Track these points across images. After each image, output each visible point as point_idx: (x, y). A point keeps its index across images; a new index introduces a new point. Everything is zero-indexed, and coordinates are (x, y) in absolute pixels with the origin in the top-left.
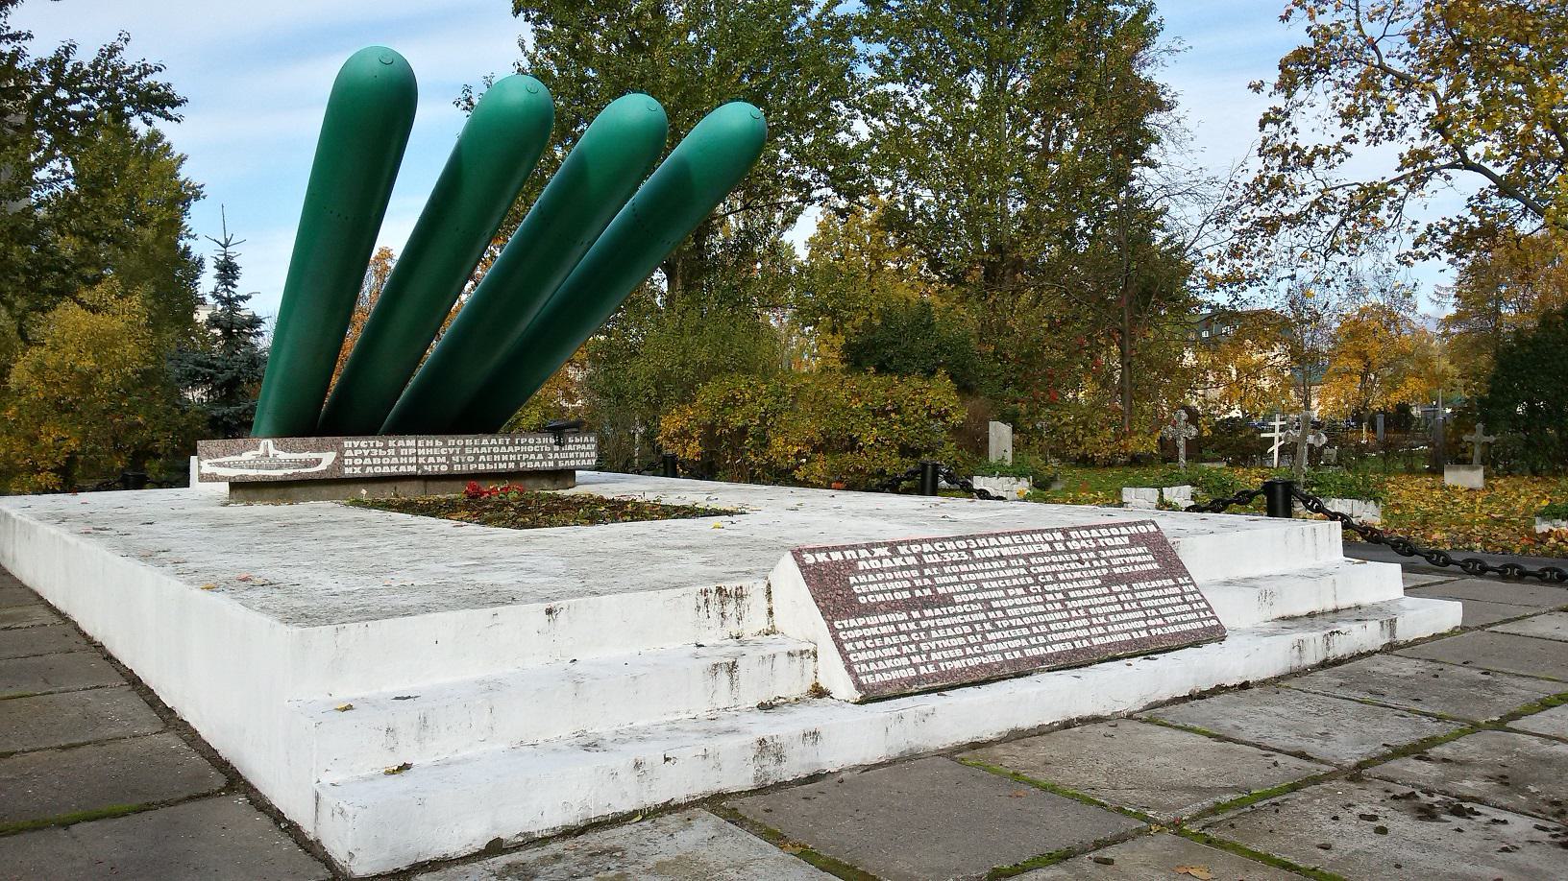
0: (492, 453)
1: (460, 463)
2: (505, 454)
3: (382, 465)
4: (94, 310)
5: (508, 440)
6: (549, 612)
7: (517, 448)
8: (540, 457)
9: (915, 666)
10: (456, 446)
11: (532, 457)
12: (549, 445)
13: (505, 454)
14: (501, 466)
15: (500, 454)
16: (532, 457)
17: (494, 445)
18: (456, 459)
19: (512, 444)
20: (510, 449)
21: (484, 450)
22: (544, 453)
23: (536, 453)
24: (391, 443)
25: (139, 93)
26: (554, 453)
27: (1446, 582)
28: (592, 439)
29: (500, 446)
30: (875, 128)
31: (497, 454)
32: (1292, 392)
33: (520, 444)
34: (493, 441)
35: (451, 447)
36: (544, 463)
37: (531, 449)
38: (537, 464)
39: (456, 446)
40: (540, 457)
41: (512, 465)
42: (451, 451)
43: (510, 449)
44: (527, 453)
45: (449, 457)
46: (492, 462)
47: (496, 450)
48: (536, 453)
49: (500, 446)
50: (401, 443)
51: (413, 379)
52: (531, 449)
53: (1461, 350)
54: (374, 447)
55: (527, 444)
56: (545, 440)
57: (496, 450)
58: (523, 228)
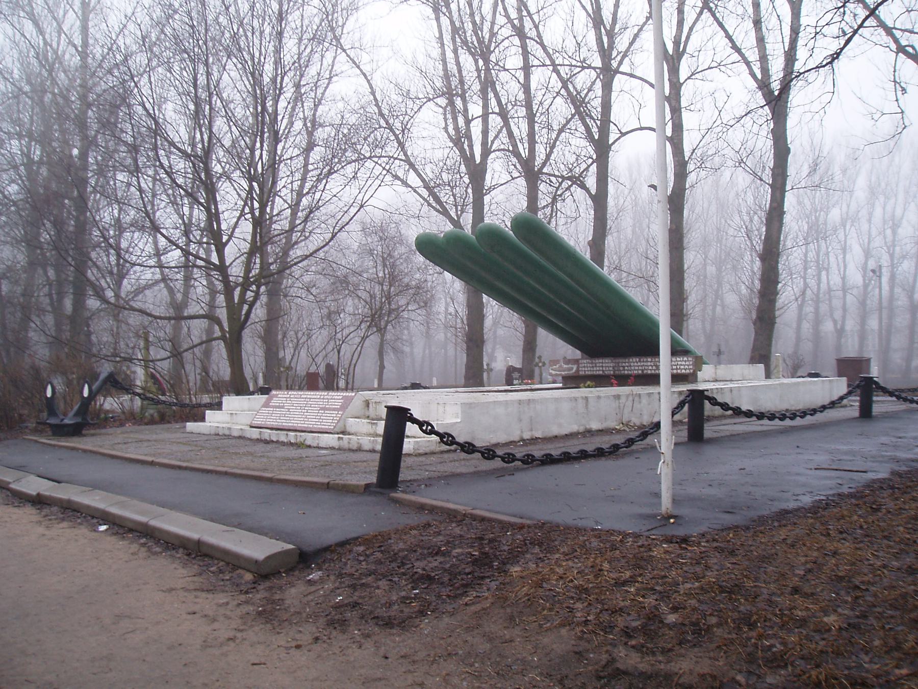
3: (677, 369)
4: (851, 479)
7: (642, 364)
8: (654, 368)
9: (603, 371)
11: (650, 368)
16: (650, 368)
19: (640, 361)
20: (639, 364)
25: (100, 129)
27: (234, 468)
28: (690, 359)
32: (175, 401)
37: (649, 364)
38: (653, 372)
41: (640, 372)
43: (639, 364)
45: (613, 367)
48: (652, 366)
50: (597, 361)
51: (537, 309)
52: (649, 364)
55: (647, 361)
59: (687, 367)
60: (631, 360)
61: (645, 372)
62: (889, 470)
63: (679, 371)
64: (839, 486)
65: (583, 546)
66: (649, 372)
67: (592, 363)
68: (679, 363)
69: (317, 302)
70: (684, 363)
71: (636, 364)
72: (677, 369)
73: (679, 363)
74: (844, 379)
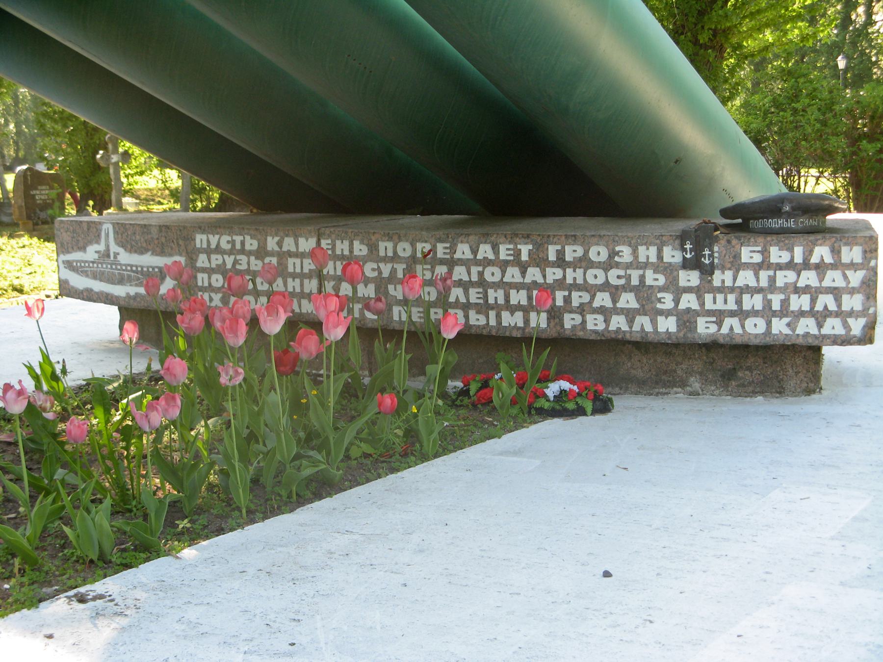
0: (482, 283)
1: (405, 302)
2: (518, 287)
3: (768, 313)
5: (525, 250)
6: (658, 574)
8: (628, 300)
10: (395, 258)
11: (603, 299)
12: (660, 267)
13: (518, 287)
14: (507, 319)
15: (507, 287)
16: (603, 299)
17: (487, 262)
18: (396, 292)
19: (541, 262)
20: (534, 274)
21: (460, 273)
22: (643, 291)
23: (615, 292)
24: (272, 243)
26: (678, 293)
29: (504, 265)
30: (52, 387)
31: (496, 286)
33: (561, 262)
34: (485, 251)
35: (385, 259)
36: (643, 323)
37: (596, 277)
38: (618, 322)
39: (395, 258)
40: (628, 300)
42: (386, 270)
44: (585, 287)
46: (484, 308)
47: (492, 274)
48: (615, 292)
49: (504, 265)
50: (289, 244)
52: (596, 277)
53: (828, 242)
54: (243, 251)
55: (584, 262)
56: (648, 253)
57: (492, 274)
58: (69, 108)
59: (826, 301)
60: (463, 250)
61: (570, 321)
62: (164, 263)
63: (779, 326)
64: (248, 460)
65: (78, 241)
66: (595, 323)
67: (261, 253)
68: (784, 278)
69: (126, 231)
70: (809, 278)
71: (513, 274)
72: (768, 313)
73: (784, 278)
74: (783, 286)
